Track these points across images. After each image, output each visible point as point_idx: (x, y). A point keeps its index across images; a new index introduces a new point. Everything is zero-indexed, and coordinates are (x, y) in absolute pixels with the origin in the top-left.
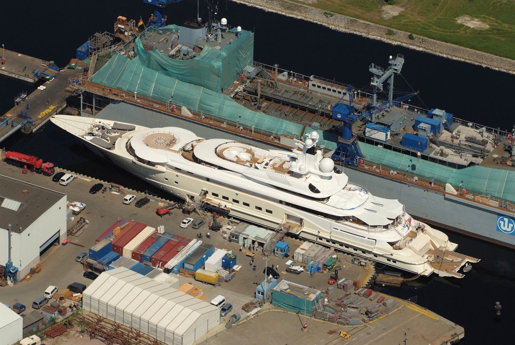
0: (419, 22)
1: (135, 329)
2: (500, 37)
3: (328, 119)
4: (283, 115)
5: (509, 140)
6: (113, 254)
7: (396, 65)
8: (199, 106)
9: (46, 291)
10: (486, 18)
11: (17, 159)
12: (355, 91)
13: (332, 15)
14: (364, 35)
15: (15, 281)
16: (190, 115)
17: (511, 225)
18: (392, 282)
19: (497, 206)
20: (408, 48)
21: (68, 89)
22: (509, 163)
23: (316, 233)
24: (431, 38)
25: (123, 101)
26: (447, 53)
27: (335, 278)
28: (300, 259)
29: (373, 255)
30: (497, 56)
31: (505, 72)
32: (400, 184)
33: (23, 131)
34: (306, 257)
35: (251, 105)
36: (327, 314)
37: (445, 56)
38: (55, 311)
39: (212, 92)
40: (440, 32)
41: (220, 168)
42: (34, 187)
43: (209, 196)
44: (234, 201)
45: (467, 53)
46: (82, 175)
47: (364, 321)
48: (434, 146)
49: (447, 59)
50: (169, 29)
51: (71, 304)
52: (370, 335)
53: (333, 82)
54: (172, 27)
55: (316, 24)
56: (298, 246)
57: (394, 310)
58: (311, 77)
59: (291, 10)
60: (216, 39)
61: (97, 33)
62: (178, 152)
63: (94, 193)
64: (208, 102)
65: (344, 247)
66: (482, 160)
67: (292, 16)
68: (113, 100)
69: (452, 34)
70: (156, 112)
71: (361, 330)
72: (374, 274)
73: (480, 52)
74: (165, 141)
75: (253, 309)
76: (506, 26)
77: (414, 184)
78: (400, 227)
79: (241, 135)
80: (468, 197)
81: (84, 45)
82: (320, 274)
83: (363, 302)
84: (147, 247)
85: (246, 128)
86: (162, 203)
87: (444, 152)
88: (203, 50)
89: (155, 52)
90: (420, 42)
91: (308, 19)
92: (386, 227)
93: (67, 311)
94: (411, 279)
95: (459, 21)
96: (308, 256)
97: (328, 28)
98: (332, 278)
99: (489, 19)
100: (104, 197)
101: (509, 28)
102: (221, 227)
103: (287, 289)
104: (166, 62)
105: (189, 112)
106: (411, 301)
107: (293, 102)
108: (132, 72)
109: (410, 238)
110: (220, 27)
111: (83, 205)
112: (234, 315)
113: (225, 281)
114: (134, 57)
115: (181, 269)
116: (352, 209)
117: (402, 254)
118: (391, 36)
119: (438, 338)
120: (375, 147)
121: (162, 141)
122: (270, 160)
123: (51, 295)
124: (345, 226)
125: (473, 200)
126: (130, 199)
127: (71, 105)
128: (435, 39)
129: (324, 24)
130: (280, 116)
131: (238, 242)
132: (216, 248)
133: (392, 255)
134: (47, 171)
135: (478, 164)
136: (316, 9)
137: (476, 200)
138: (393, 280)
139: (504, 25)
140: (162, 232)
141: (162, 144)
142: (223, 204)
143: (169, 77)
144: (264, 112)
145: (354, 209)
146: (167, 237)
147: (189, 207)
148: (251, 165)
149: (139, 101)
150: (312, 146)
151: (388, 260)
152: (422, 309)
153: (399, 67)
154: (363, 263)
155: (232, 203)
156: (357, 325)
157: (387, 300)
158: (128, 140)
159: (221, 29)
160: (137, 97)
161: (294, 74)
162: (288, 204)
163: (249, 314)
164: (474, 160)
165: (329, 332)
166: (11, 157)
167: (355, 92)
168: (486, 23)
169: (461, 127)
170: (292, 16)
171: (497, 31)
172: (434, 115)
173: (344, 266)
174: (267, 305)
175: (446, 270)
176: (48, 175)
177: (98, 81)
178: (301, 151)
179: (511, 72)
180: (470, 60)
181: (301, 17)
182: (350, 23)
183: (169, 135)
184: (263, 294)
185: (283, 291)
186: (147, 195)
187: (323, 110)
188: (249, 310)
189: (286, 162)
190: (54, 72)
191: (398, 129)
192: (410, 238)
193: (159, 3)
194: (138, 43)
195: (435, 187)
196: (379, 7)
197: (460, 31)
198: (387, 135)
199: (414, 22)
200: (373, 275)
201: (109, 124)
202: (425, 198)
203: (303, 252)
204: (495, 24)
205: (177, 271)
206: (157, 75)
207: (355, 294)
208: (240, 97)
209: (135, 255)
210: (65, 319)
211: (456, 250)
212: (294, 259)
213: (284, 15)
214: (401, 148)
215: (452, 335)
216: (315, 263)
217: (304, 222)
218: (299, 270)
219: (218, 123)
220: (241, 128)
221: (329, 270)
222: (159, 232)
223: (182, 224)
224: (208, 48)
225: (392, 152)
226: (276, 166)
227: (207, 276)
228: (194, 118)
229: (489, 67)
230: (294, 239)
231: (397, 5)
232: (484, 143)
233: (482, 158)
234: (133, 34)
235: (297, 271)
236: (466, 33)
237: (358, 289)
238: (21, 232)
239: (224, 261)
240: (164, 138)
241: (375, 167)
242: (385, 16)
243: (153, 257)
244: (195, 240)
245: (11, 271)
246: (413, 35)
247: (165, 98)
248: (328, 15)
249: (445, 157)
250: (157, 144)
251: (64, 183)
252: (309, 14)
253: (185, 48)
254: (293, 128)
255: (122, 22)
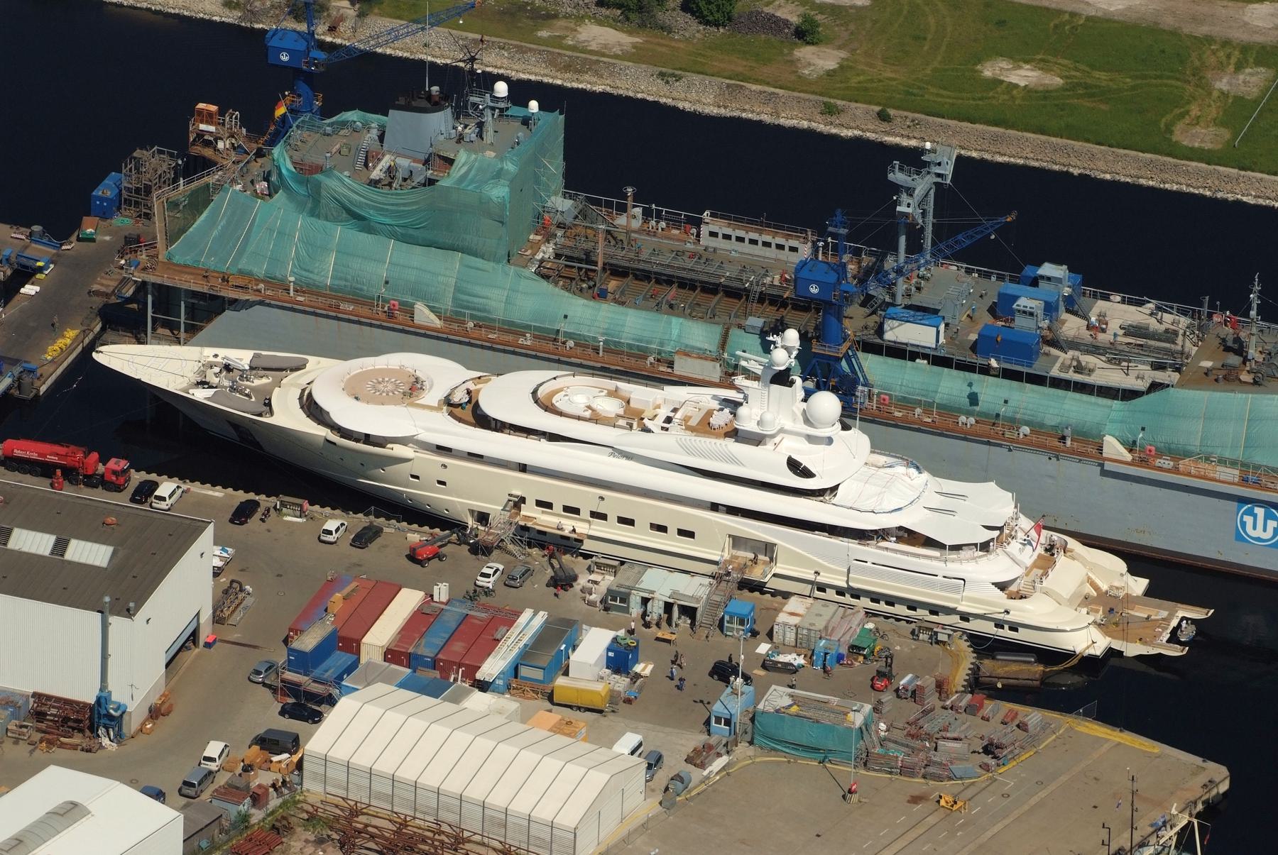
0: (894, 79)
1: (450, 825)
2: (1095, 102)
3: (776, 308)
4: (665, 307)
5: (1226, 325)
6: (339, 659)
7: (939, 164)
8: (454, 299)
9: (206, 754)
10: (1048, 62)
11: (34, 456)
12: (819, 241)
13: (678, 78)
14: (766, 118)
15: (119, 738)
16: (438, 323)
17: (1272, 524)
18: (1020, 677)
19: (1236, 480)
20: (881, 143)
21: (95, 287)
22: (1245, 377)
23: (811, 577)
24: (933, 116)
25: (261, 303)
26: (979, 148)
27: (885, 675)
28: (790, 637)
29: (958, 617)
30: (1102, 147)
31: (1128, 182)
32: (986, 447)
33: (16, 393)
34: (805, 632)
35: (581, 290)
36: (897, 757)
37: (974, 154)
38: (244, 798)
39: (486, 262)
40: (951, 101)
41: (554, 437)
42: (126, 510)
43: (529, 510)
44: (594, 515)
45: (1027, 144)
46: (197, 483)
47: (986, 767)
48: (1054, 351)
49: (983, 161)
50: (348, 122)
51: (277, 780)
52: (1010, 799)
53: (762, 222)
54: (352, 116)
55: (644, 101)
56: (778, 611)
57: (1047, 739)
58: (705, 214)
59: (575, 72)
60: (480, 135)
61: (138, 151)
62: (438, 409)
63: (242, 524)
64: (478, 290)
65: (882, 603)
66: (1176, 376)
67: (580, 86)
68: (236, 300)
69: (980, 103)
70: (349, 321)
71: (984, 789)
72: (974, 661)
73: (1059, 140)
74: (397, 386)
75: (713, 761)
76: (1102, 77)
77: (1022, 444)
78: (1014, 547)
79: (573, 360)
80: (1160, 465)
81: (106, 181)
82: (845, 669)
83: (970, 726)
84: (417, 635)
85: (583, 344)
86: (416, 536)
87: (1083, 364)
88: (455, 164)
89: (328, 176)
90: (909, 127)
91: (621, 92)
92: (985, 547)
93: (270, 798)
94: (1060, 667)
95: (988, 73)
96: (809, 630)
97: (675, 109)
98: (880, 674)
99: (1056, 63)
100: (269, 531)
101: (1111, 80)
102: (575, 578)
103: (790, 706)
104: (362, 199)
105: (432, 316)
106: (1087, 714)
107: (684, 274)
108: (271, 230)
109: (1040, 572)
110: (492, 104)
111: (227, 552)
112: (678, 775)
113: (624, 702)
114: (270, 195)
115: (513, 681)
116: (896, 510)
117: (1027, 606)
118: (834, 117)
119: (1172, 793)
120: (909, 363)
121: (390, 387)
122: (675, 410)
123: (218, 763)
124: (885, 553)
125: (1176, 470)
126: (337, 530)
127: (113, 326)
128: (943, 118)
129: (663, 100)
130: (658, 308)
131: (626, 610)
132: (584, 627)
133: (1007, 612)
134: (114, 478)
135: (1172, 386)
136: (636, 65)
137: (1181, 469)
138: (1021, 670)
139: (1097, 74)
140: (444, 598)
141: (391, 394)
142: (568, 525)
143: (370, 236)
144: (616, 301)
145: (900, 509)
146: (460, 610)
147: (491, 538)
148: (631, 426)
149: (299, 298)
150: (787, 364)
151: (997, 626)
152: (1114, 731)
153: (948, 167)
154: (941, 637)
155: (589, 522)
156: (970, 778)
157: (1027, 716)
158: (300, 391)
159: (493, 109)
160: (296, 291)
161: (660, 212)
162: (733, 511)
163: (705, 773)
164: (1160, 376)
165: (908, 798)
166: (18, 453)
167: (821, 244)
168: (1052, 73)
169: (1101, 305)
170: (580, 86)
171: (1086, 88)
172: (1042, 277)
173: (898, 648)
174: (742, 749)
175: (1140, 640)
176: (118, 489)
177: (188, 260)
178: (755, 380)
179: (1143, 182)
180: (1037, 160)
181: (603, 87)
182: (726, 92)
183: (401, 371)
184: (728, 722)
185: (782, 710)
186: (372, 517)
187: (764, 289)
188: (706, 761)
189: (715, 412)
190: (48, 252)
191: (957, 317)
192: (1040, 572)
193: (307, 63)
194: (281, 160)
195: (1075, 446)
196: (786, 51)
197: (996, 95)
198: (938, 332)
199: (880, 81)
200: (972, 664)
201: (242, 357)
202: (1050, 477)
203: (794, 620)
204: (1073, 73)
205: (503, 685)
206: (340, 232)
207: (944, 708)
208: (551, 272)
209: (392, 655)
210: (269, 815)
211: (1149, 593)
212: (775, 640)
213: (559, 86)
214: (976, 361)
215: (1205, 786)
216: (831, 643)
217: (780, 554)
218: (796, 663)
219: (510, 338)
220: (571, 343)
221: (865, 657)
222: (436, 598)
223: (479, 578)
224: (468, 158)
225: (954, 372)
226: (693, 422)
227: (583, 690)
228: (447, 330)
229: (1088, 172)
230: (757, 594)
231: (827, 44)
232: (1170, 336)
233: (1178, 370)
234: (236, 145)
235: (792, 665)
236: (1013, 97)
237: (948, 698)
238: (134, 615)
239: (611, 654)
240: (393, 380)
241: (918, 411)
242: (806, 72)
243: (440, 656)
244: (528, 613)
245: (112, 711)
246: (888, 110)
247: (365, 288)
248: (669, 79)
249: (1089, 375)
250: (378, 393)
251: (163, 505)
252: (620, 80)
253: (404, 163)
254: (700, 334)
255: (209, 118)
